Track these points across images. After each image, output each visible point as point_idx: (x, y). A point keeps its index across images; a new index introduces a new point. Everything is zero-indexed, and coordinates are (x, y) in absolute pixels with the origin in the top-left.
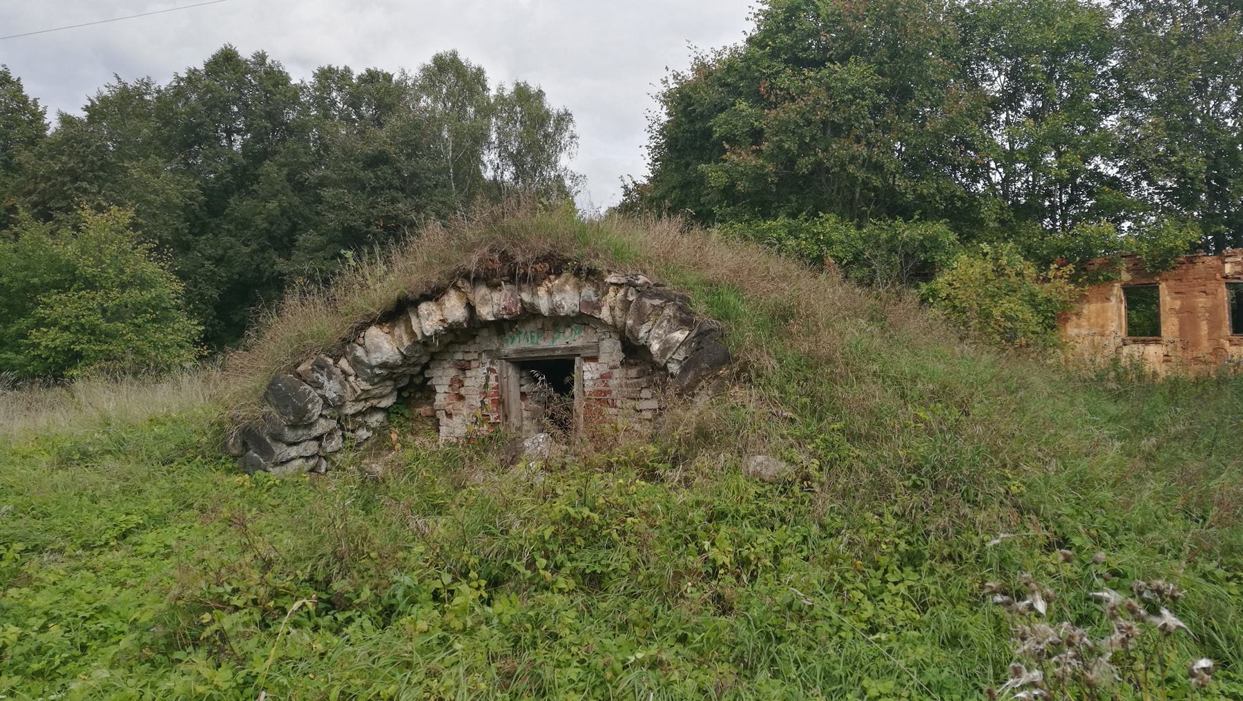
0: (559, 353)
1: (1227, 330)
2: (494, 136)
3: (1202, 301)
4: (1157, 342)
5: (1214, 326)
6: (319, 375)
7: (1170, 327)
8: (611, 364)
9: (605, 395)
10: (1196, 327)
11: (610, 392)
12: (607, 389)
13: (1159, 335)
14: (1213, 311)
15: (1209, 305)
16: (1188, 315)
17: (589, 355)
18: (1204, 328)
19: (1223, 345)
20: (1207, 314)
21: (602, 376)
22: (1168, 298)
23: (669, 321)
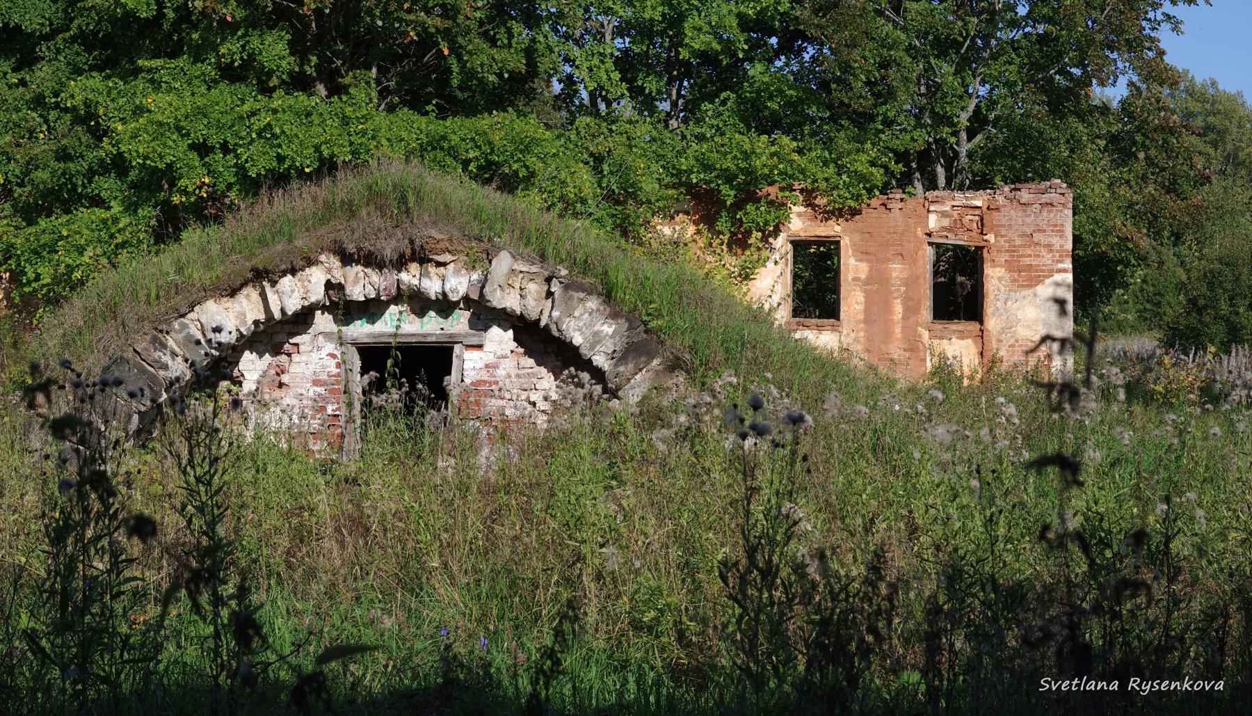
0: (434, 339)
1: (926, 313)
2: (215, 24)
3: (897, 270)
4: (834, 329)
5: (911, 310)
6: (161, 354)
7: (852, 302)
8: (499, 354)
9: (490, 386)
10: (888, 309)
11: (496, 383)
12: (493, 379)
13: (838, 318)
14: (911, 282)
15: (904, 275)
16: (877, 286)
17: (475, 343)
18: (898, 309)
19: (920, 336)
20: (903, 289)
21: (487, 366)
22: (852, 261)
23: (590, 314)
